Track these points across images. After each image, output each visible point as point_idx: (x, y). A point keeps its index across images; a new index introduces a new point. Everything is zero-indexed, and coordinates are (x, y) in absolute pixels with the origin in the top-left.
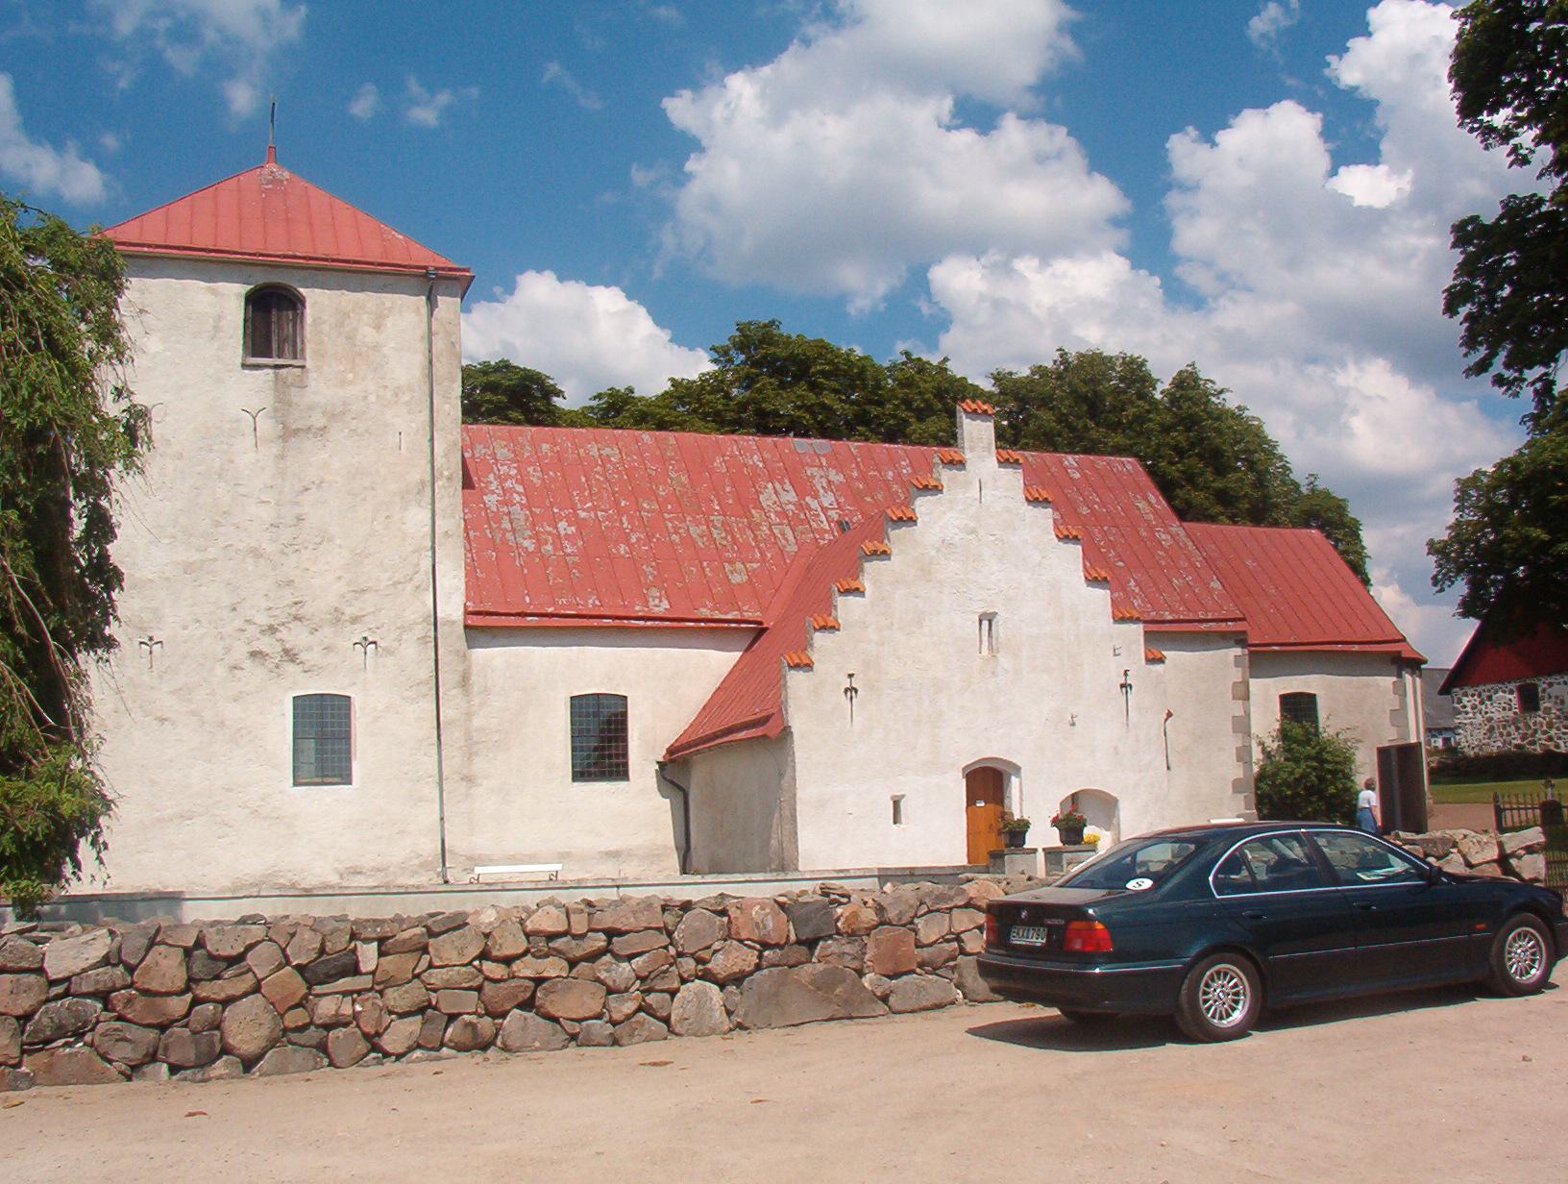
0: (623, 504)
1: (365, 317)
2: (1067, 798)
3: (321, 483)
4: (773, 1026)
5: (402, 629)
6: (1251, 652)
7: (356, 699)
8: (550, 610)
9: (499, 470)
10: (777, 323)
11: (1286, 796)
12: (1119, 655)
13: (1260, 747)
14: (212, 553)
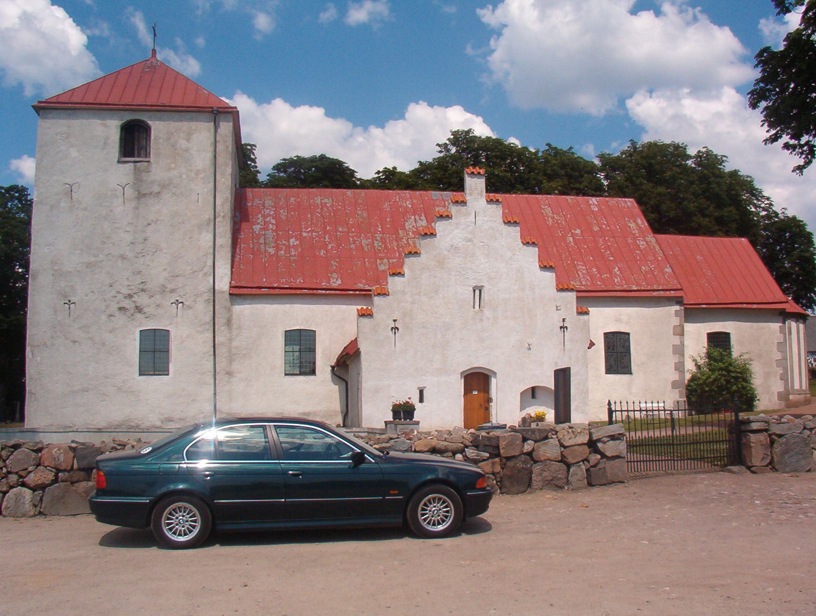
0: (328, 229)
1: (182, 135)
2: (529, 388)
3: (157, 221)
4: (60, 515)
5: (197, 295)
6: (685, 308)
7: (172, 332)
8: (275, 285)
9: (264, 212)
10: (472, 131)
11: (706, 391)
12: (560, 310)
13: (694, 362)
14: (101, 257)
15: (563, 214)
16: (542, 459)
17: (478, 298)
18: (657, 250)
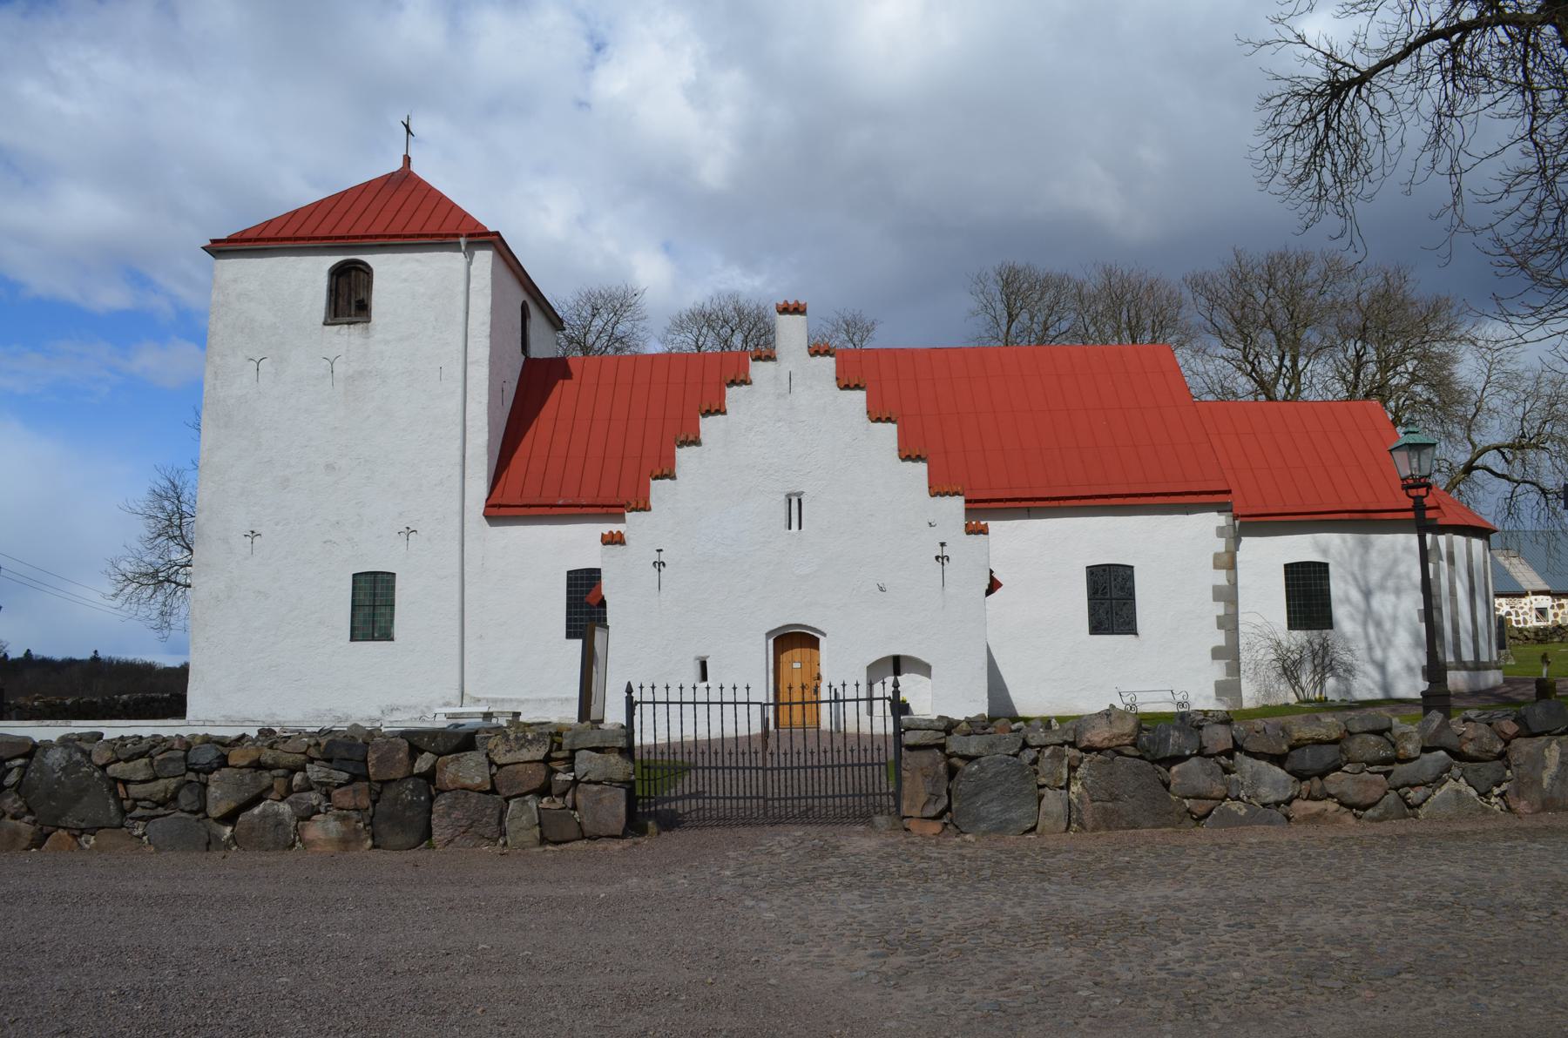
16: (451, 786)
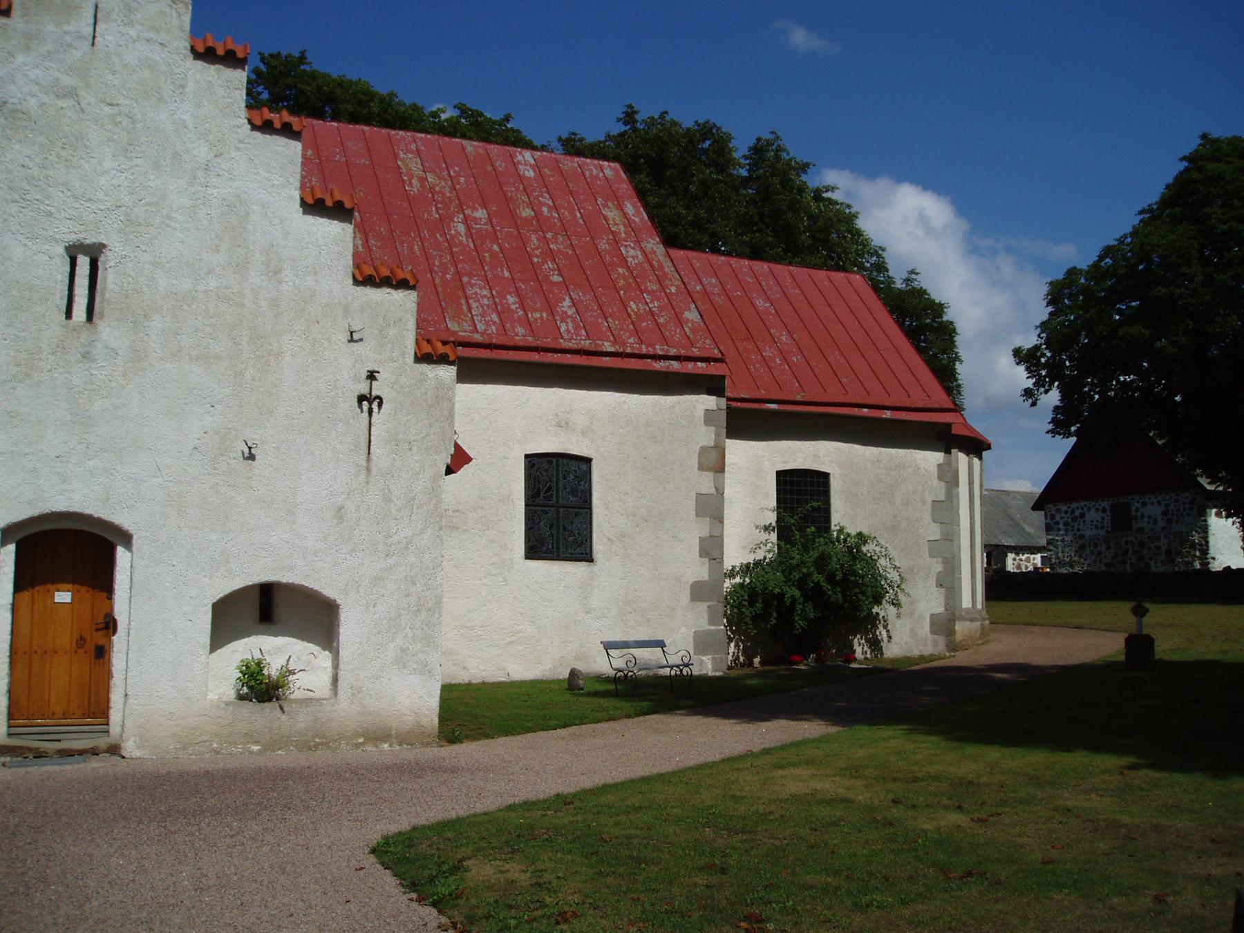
15: (449, 175)
17: (86, 282)
18: (667, 270)
